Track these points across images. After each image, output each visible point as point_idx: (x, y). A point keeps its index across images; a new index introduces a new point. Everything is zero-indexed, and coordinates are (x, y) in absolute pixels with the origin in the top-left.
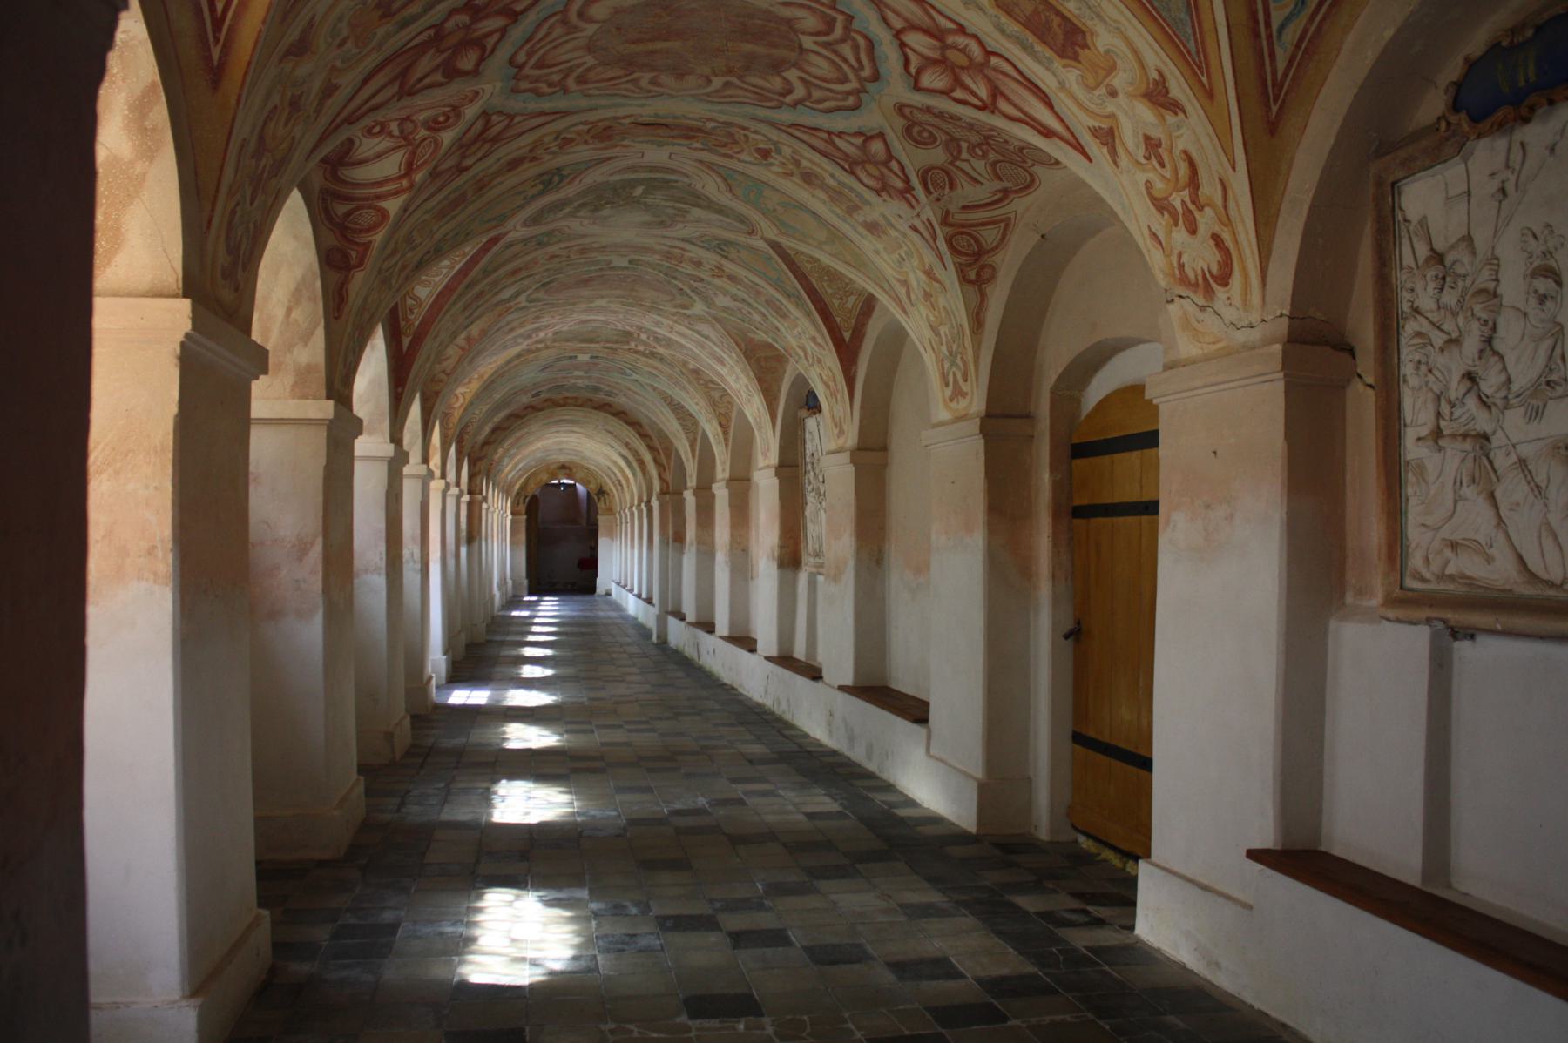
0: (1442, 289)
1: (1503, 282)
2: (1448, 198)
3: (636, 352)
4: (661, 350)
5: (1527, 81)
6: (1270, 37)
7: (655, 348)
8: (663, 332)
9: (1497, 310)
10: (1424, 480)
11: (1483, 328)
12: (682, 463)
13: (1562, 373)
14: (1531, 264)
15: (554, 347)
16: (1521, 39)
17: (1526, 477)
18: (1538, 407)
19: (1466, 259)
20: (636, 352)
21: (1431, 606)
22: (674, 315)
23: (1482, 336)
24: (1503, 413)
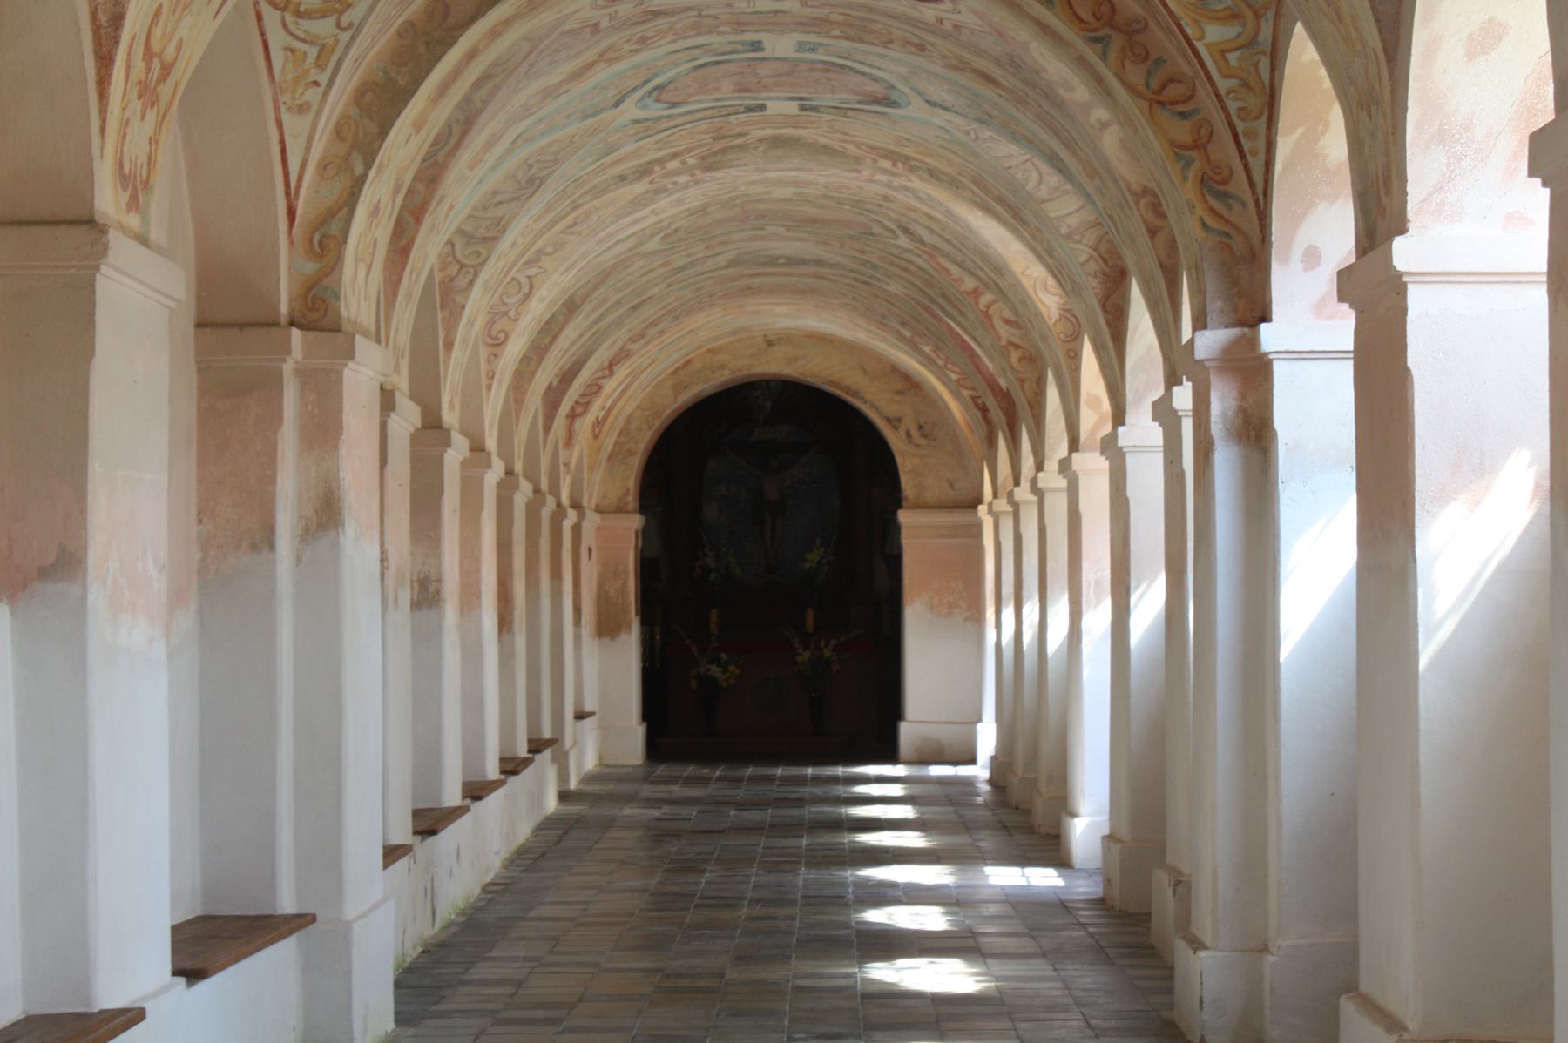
3: (675, 156)
4: (640, 188)
7: (651, 182)
8: (663, 202)
12: (363, 182)
15: (858, 145)
20: (675, 156)
22: (670, 224)
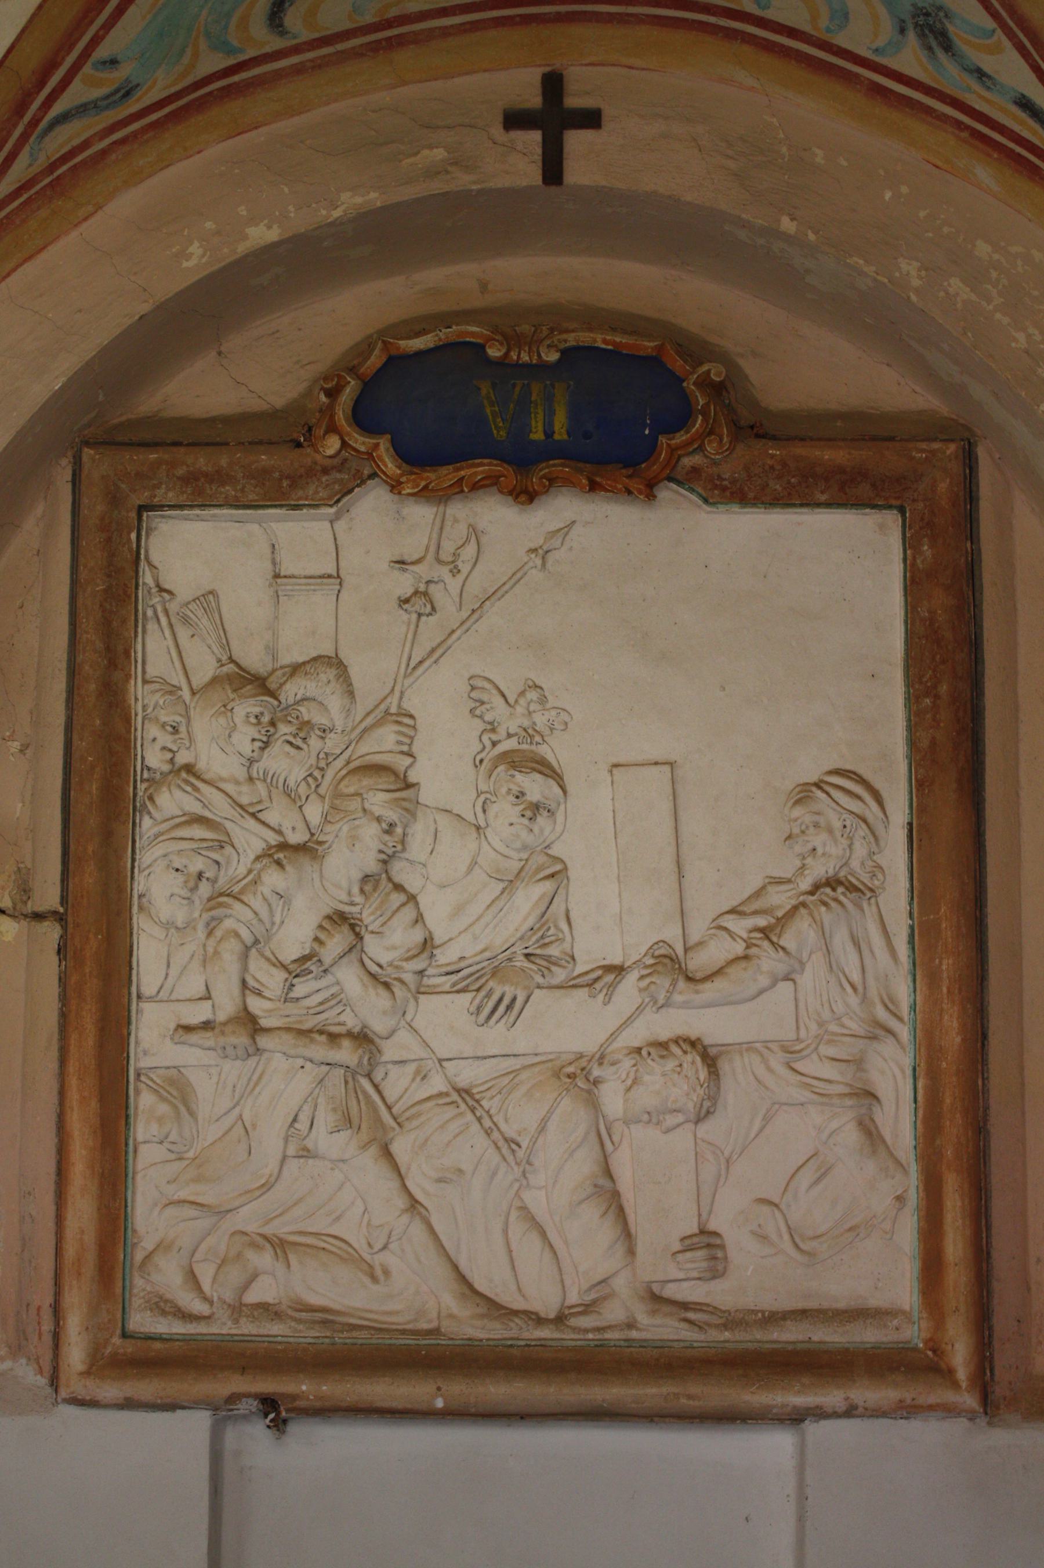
0: (266, 745)
1: (422, 760)
2: (277, 576)
5: (549, 434)
6: (34, 123)
9: (411, 809)
10: (192, 1113)
11: (387, 838)
13: (567, 946)
14: (494, 744)
16: (525, 357)
17: (479, 1120)
18: (514, 999)
19: (335, 703)
21: (243, 1370)
23: (381, 851)
24: (416, 1000)
